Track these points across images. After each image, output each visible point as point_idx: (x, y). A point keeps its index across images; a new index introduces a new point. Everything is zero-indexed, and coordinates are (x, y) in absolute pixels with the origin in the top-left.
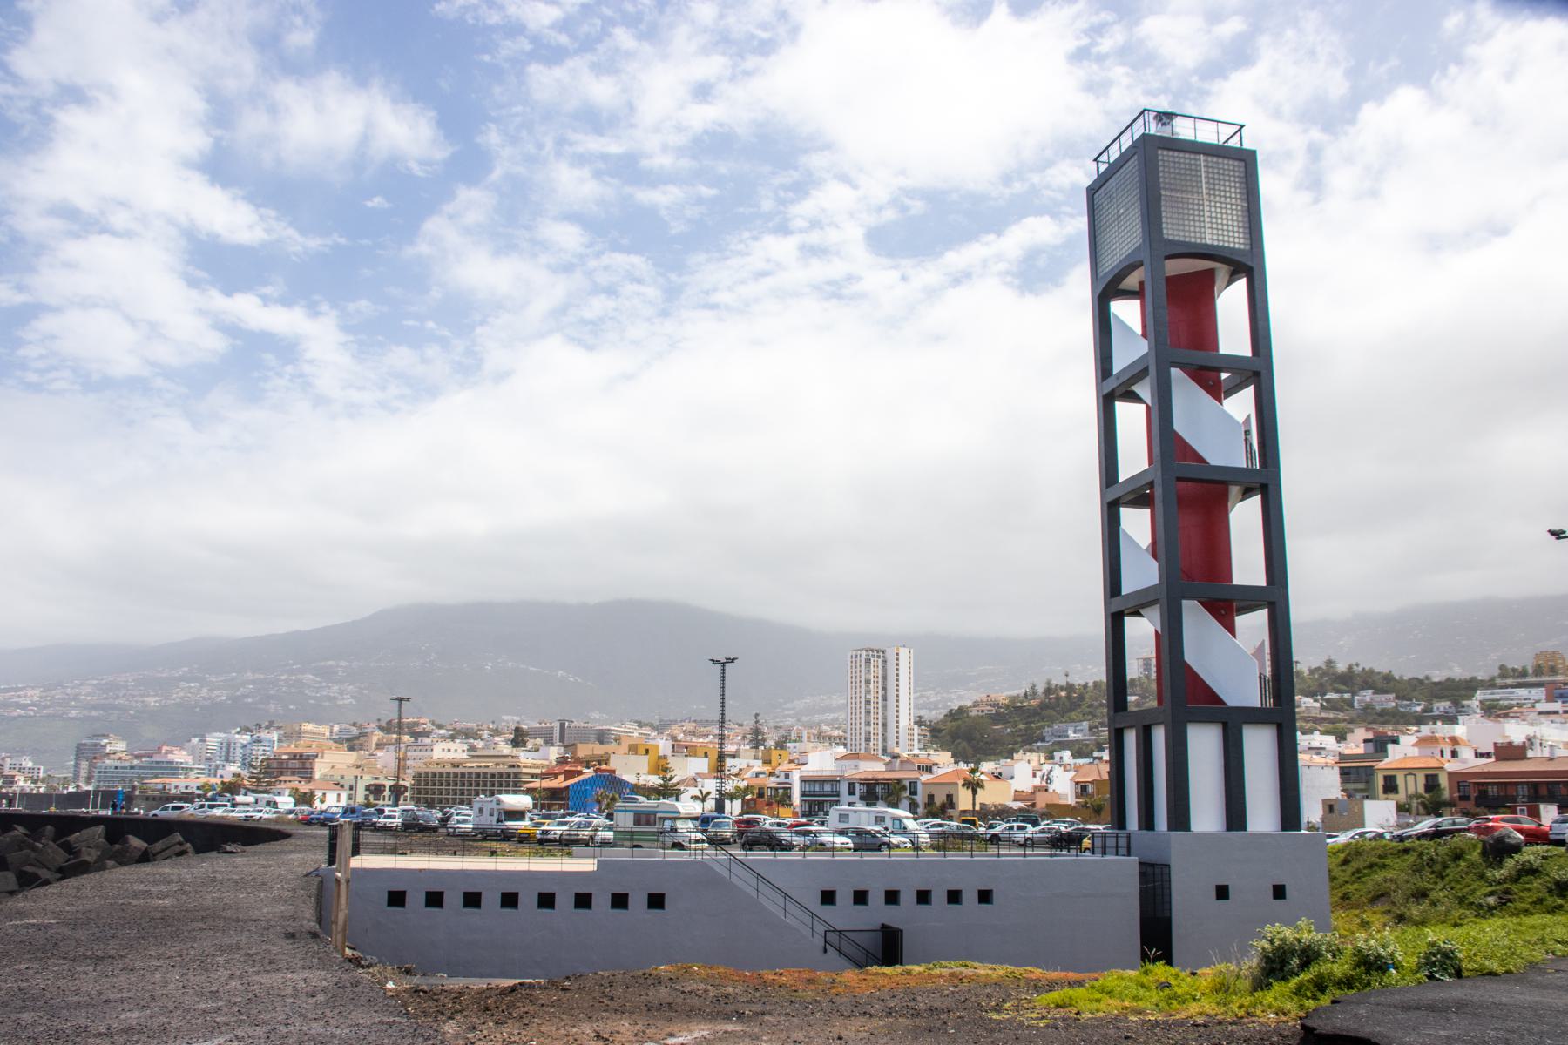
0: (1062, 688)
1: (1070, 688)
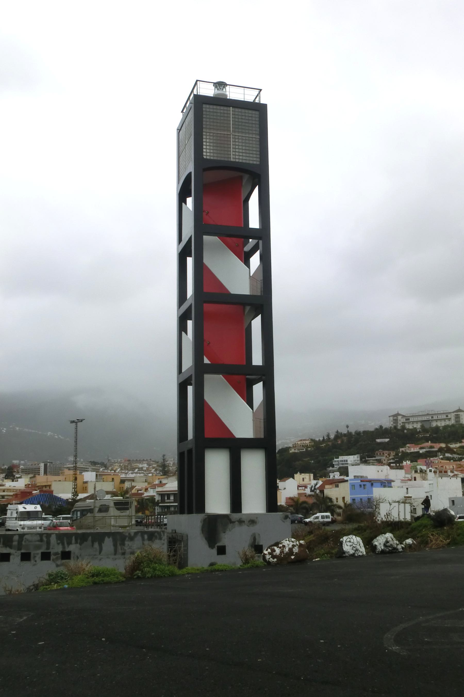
0: (345, 435)
1: (349, 435)
